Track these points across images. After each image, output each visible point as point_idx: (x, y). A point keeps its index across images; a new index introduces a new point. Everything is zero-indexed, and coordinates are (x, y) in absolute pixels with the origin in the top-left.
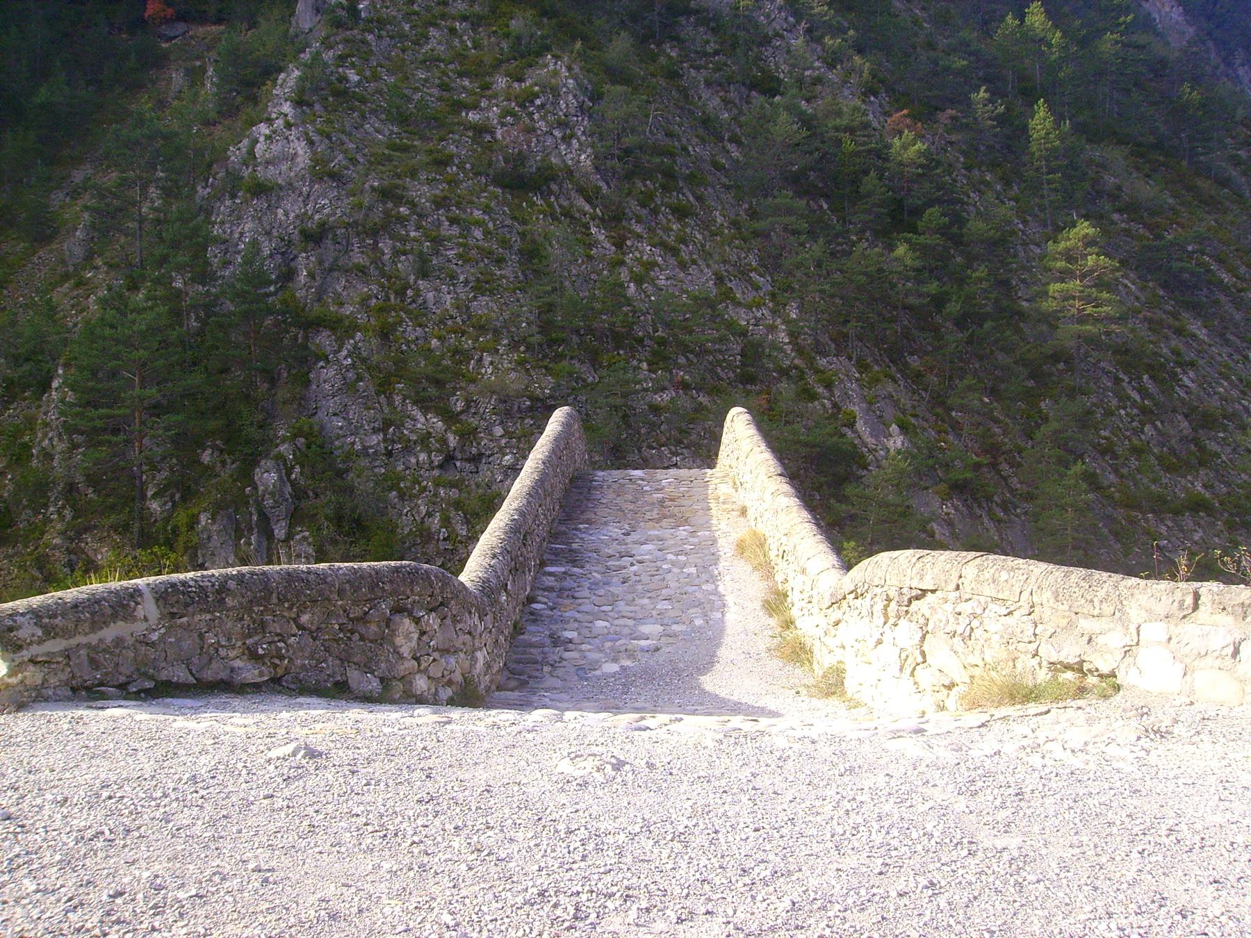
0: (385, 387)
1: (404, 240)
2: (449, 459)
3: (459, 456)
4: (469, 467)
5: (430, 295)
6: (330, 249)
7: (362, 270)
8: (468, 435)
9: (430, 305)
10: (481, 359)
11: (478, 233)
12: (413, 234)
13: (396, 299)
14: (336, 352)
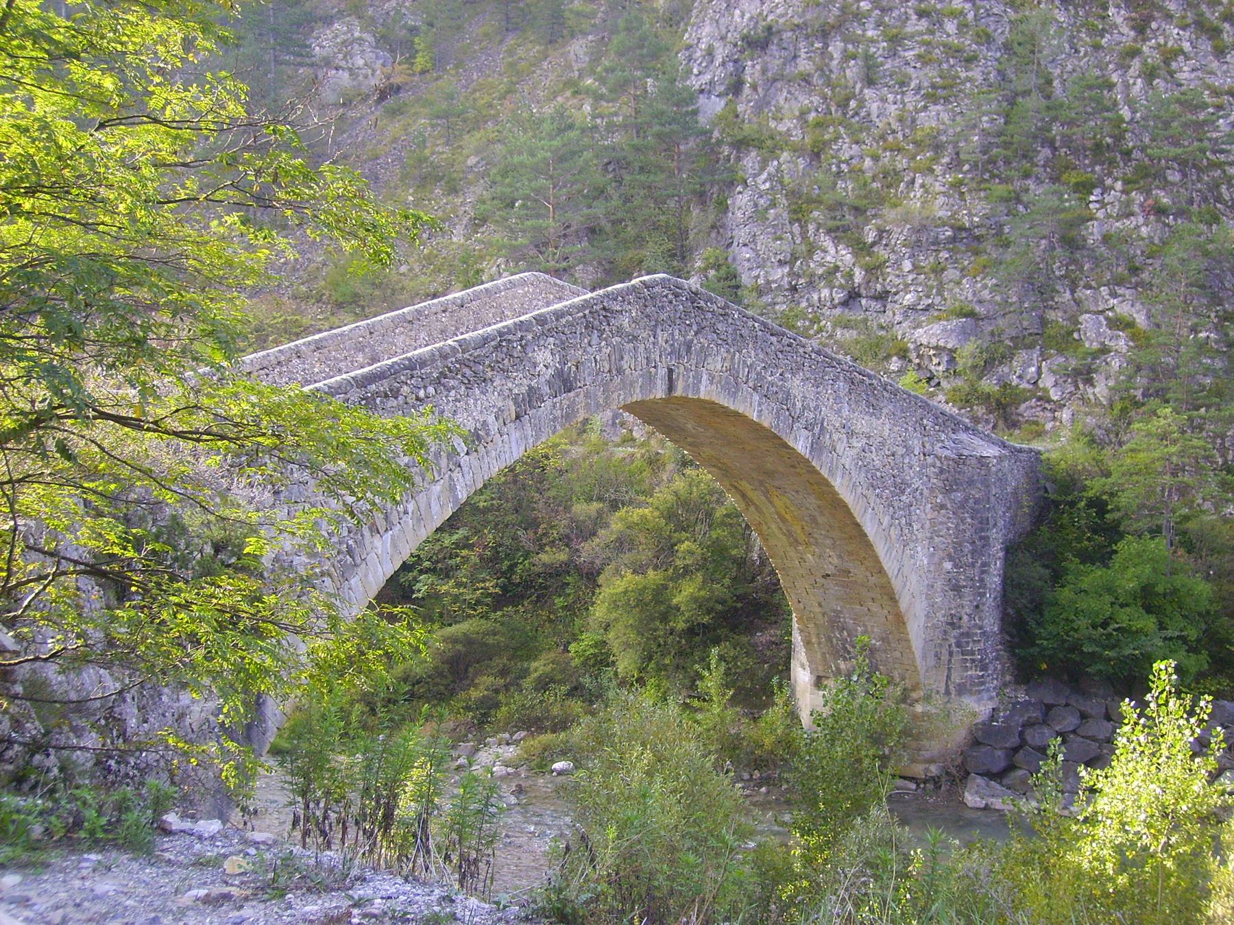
0: (798, 215)
1: (856, 41)
2: (853, 297)
3: (863, 292)
4: (877, 306)
6: (774, 58)
7: (806, 79)
8: (873, 271)
9: (874, 117)
10: (913, 182)
11: (951, 27)
12: (870, 34)
13: (837, 111)
14: (755, 176)
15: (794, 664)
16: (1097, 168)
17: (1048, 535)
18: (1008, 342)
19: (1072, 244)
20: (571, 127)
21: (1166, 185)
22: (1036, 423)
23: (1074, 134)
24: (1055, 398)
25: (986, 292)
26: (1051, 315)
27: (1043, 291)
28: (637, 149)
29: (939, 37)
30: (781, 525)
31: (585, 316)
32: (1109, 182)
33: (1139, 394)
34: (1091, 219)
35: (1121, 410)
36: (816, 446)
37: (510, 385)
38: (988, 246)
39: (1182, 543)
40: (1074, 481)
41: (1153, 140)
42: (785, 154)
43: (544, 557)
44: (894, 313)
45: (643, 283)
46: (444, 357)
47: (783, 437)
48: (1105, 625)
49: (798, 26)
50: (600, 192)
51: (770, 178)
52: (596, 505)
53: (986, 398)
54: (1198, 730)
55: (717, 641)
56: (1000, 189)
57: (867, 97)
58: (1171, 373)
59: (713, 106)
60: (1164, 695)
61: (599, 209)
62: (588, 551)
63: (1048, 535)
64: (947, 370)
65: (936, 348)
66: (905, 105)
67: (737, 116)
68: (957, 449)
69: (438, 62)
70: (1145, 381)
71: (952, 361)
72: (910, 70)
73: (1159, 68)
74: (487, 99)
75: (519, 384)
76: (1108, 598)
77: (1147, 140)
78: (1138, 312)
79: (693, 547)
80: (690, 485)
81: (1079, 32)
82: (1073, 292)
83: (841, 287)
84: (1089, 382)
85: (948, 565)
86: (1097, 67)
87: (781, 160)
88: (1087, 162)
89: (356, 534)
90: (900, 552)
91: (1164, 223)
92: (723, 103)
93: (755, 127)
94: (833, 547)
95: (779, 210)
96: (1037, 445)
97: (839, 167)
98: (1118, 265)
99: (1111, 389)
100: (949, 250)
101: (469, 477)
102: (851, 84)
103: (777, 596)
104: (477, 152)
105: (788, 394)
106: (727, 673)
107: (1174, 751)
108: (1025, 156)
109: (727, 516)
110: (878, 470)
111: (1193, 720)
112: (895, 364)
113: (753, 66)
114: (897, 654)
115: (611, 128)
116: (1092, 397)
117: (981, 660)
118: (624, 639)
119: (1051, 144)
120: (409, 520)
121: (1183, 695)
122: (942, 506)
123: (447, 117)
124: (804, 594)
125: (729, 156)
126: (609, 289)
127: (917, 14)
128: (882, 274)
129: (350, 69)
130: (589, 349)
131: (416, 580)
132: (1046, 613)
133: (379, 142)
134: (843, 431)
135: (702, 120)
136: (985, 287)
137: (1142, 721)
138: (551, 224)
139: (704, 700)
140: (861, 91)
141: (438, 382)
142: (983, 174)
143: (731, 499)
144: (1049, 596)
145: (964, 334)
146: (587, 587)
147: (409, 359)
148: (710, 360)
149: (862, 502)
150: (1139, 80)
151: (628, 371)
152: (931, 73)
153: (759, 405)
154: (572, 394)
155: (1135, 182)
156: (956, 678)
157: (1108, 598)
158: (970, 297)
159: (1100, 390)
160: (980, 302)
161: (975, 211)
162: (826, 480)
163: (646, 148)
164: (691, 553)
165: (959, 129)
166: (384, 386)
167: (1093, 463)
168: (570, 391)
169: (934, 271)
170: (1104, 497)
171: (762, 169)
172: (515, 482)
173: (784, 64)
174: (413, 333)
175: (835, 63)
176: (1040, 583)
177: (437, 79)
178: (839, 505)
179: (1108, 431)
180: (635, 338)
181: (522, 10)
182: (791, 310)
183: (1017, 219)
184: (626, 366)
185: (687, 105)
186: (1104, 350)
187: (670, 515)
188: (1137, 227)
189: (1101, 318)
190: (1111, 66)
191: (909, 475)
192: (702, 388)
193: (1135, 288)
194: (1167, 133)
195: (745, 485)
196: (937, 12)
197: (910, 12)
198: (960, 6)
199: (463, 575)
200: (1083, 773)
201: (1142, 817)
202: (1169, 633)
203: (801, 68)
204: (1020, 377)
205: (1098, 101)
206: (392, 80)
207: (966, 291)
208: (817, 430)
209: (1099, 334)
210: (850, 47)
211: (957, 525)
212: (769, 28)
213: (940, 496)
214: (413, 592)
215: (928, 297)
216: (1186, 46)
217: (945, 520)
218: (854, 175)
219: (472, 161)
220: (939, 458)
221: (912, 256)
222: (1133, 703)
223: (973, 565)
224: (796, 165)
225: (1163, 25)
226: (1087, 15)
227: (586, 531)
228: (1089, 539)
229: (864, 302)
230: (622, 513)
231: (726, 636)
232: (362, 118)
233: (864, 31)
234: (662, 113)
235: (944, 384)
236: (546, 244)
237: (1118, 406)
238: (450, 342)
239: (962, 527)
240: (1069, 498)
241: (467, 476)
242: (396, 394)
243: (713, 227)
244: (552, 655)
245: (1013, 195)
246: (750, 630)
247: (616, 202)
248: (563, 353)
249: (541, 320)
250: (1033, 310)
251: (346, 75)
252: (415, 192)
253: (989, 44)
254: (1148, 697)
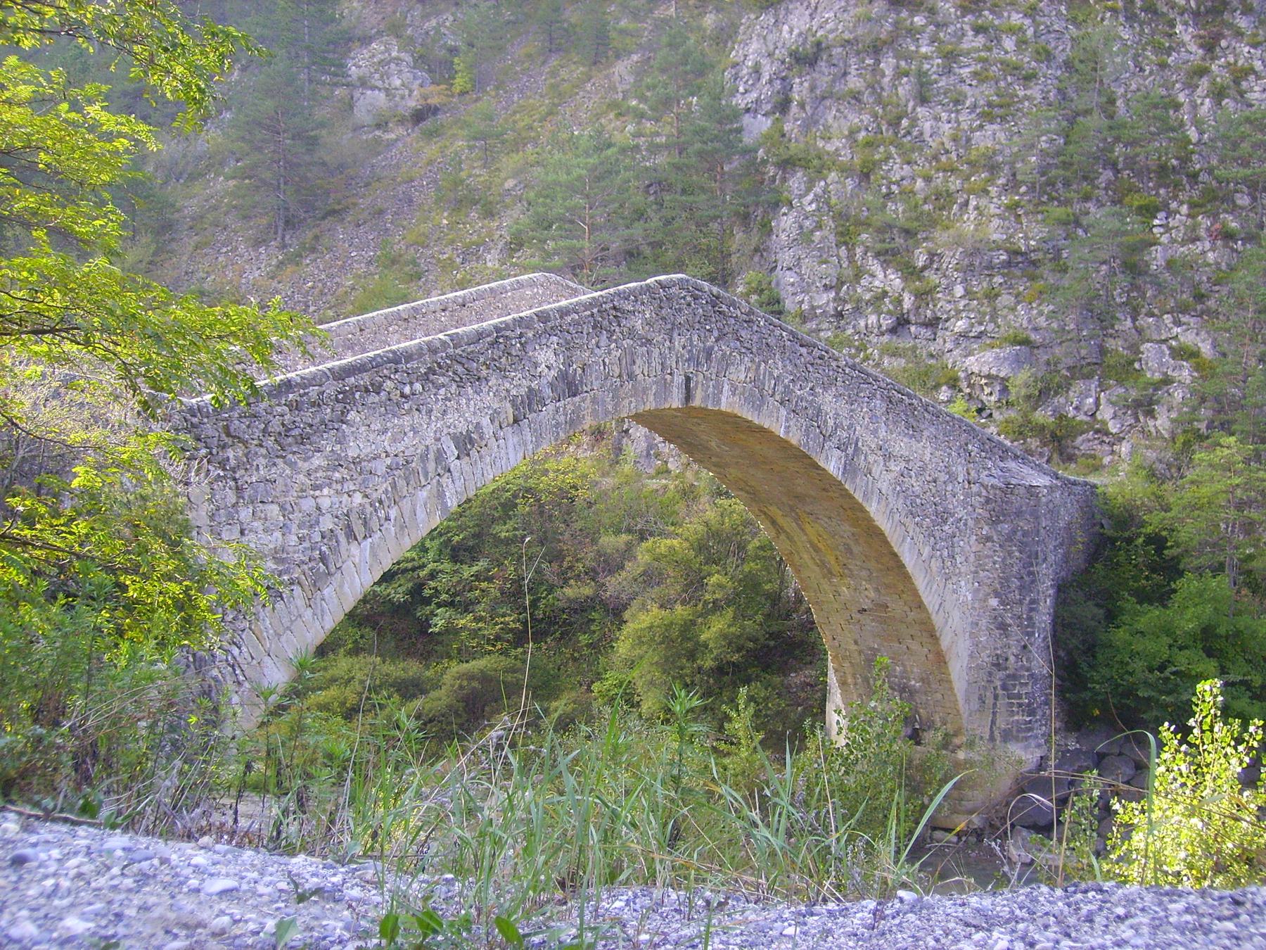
0: (845, 237)
1: (909, 58)
2: (901, 323)
3: (912, 318)
4: (926, 333)
5: (927, 125)
6: (823, 75)
7: (856, 97)
8: (924, 296)
9: (926, 136)
10: (966, 203)
11: (1009, 43)
12: (923, 50)
13: (887, 130)
14: (801, 197)
15: (830, 708)
16: (1162, 191)
17: (1102, 573)
18: (1064, 372)
19: (1134, 269)
20: (610, 146)
21: (1234, 209)
22: (1094, 457)
23: (1137, 155)
24: (1114, 431)
25: (1043, 319)
26: (1111, 344)
27: (1104, 320)
28: (677, 168)
29: (996, 54)
30: (814, 554)
31: (592, 315)
32: (1174, 205)
33: (1203, 426)
34: (1155, 244)
35: (1184, 444)
36: (850, 468)
37: (507, 385)
38: (1045, 270)
39: (1248, 585)
40: (1132, 517)
41: (1222, 161)
42: (833, 174)
43: (569, 592)
44: (944, 340)
45: (659, 283)
46: (433, 351)
47: (813, 456)
48: (1162, 668)
49: (848, 41)
50: (640, 215)
51: (817, 199)
52: (624, 537)
53: (1040, 430)
54: (1247, 759)
55: (747, 681)
56: (1058, 211)
57: (920, 116)
58: (1237, 405)
59: (759, 125)
60: (1208, 720)
61: (638, 230)
62: (614, 584)
63: (1102, 573)
64: (999, 401)
65: (988, 376)
66: (959, 124)
67: (784, 135)
68: (1005, 477)
69: (478, 84)
70: (1210, 413)
71: (1005, 390)
72: (966, 88)
73: (1228, 87)
74: (527, 121)
75: (518, 385)
76: (1166, 640)
77: (1214, 162)
78: (1203, 341)
79: (724, 580)
80: (722, 515)
81: (1144, 50)
82: (1134, 320)
83: (889, 313)
84: (1150, 414)
85: (994, 602)
86: (1162, 86)
87: (829, 181)
88: (1151, 184)
89: (330, 539)
90: (942, 585)
91: (1232, 249)
92: (769, 122)
93: (802, 146)
94: (869, 579)
95: (826, 232)
96: (1093, 479)
97: (889, 188)
98: (1182, 292)
99: (1173, 421)
100: (1003, 275)
101: (459, 484)
102: (903, 102)
103: (813, 636)
104: (515, 174)
105: (820, 411)
106: (756, 715)
107: (1219, 782)
108: (1085, 178)
109: (761, 548)
110: (918, 496)
111: (1241, 748)
112: (944, 393)
113: (801, 84)
114: (939, 696)
115: (654, 149)
116: (1153, 430)
117: (1029, 705)
118: (649, 677)
119: (1114, 166)
120: (391, 528)
121: (1230, 720)
122: (989, 539)
123: (484, 139)
124: (839, 630)
125: (774, 177)
126: (621, 287)
127: (973, 30)
128: (933, 300)
129: (387, 90)
130: (597, 351)
131: (433, 614)
132: (1099, 656)
133: (415, 165)
134: (880, 453)
135: (747, 140)
136: (1041, 314)
137: (1184, 747)
138: (586, 245)
139: (732, 743)
140: (914, 109)
141: (425, 378)
142: (1040, 196)
143: (765, 532)
144: (1103, 637)
145: (1018, 362)
146: (612, 623)
147: (394, 352)
148: (732, 369)
149: (900, 530)
150: (1207, 100)
151: (640, 377)
152: (988, 91)
153: (787, 420)
154: (577, 399)
155: (1201, 206)
156: (1001, 723)
157: (1166, 640)
158: (1025, 324)
159: (1162, 422)
160: (1036, 329)
161: (1031, 234)
162: (861, 505)
163: (688, 167)
164: (720, 586)
165: (1016, 149)
166: (365, 379)
167: (1152, 498)
168: (575, 395)
169: (987, 296)
170: (1164, 533)
171: (808, 190)
172: (542, 513)
173: (834, 81)
174: (408, 332)
175: (886, 80)
176: (1093, 623)
177: (477, 100)
178: (875, 533)
179: (1169, 466)
180: (649, 341)
181: (566, 30)
182: (836, 336)
183: (1076, 243)
184: (638, 372)
185: (732, 123)
186: (1167, 381)
187: (701, 547)
188: (1204, 253)
189: (1164, 347)
190: (1177, 86)
191: (952, 503)
192: (724, 400)
193: (1200, 316)
194: (1236, 154)
195: (774, 511)
196: (996, 28)
197: (966, 27)
198: (1019, 22)
199: (481, 610)
200: (1117, 807)
201: (1182, 855)
202: (1232, 677)
203: (851, 85)
204: (1077, 408)
205: (1164, 120)
206: (429, 101)
207: (1020, 318)
208: (850, 451)
209: (1161, 364)
210: (903, 63)
211: (1004, 559)
212: (819, 44)
213: (986, 528)
214: (430, 626)
215: (981, 324)
216: (1258, 65)
217: (991, 553)
218: (904, 197)
219: (510, 183)
220: (986, 487)
221: (964, 281)
222: (1173, 728)
223: (1021, 602)
224: (844, 187)
225: (1233, 43)
226: (1153, 33)
227: (612, 565)
228: (1147, 578)
229: (913, 329)
230: (649, 544)
231: (757, 676)
232: (396, 140)
233: (918, 47)
234: (704, 130)
235: (996, 415)
236: (582, 267)
237: (1181, 439)
238: (441, 336)
239: (1008, 561)
240: (1126, 534)
241: (457, 482)
242: (378, 390)
243: (756, 250)
244: (574, 694)
245: (1072, 218)
246: (784, 670)
247: (655, 222)
248: (568, 353)
249: (543, 317)
250: (1091, 338)
251: (382, 95)
252: (450, 215)
253: (1049, 61)
254: (1191, 722)
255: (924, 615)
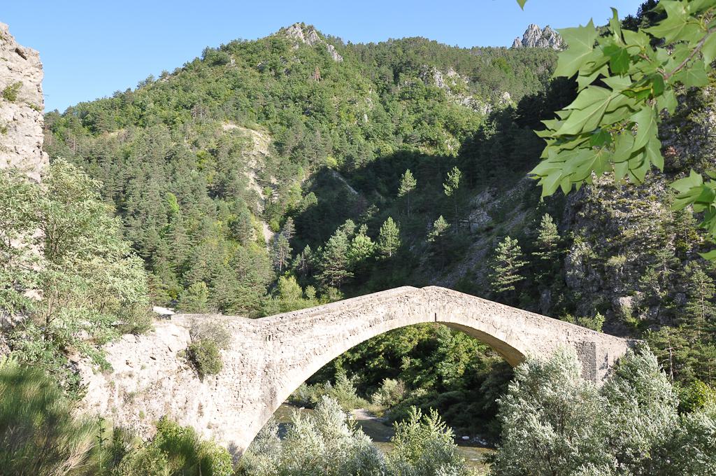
75: (371, 317)
166: (319, 317)
255: (338, 365)
